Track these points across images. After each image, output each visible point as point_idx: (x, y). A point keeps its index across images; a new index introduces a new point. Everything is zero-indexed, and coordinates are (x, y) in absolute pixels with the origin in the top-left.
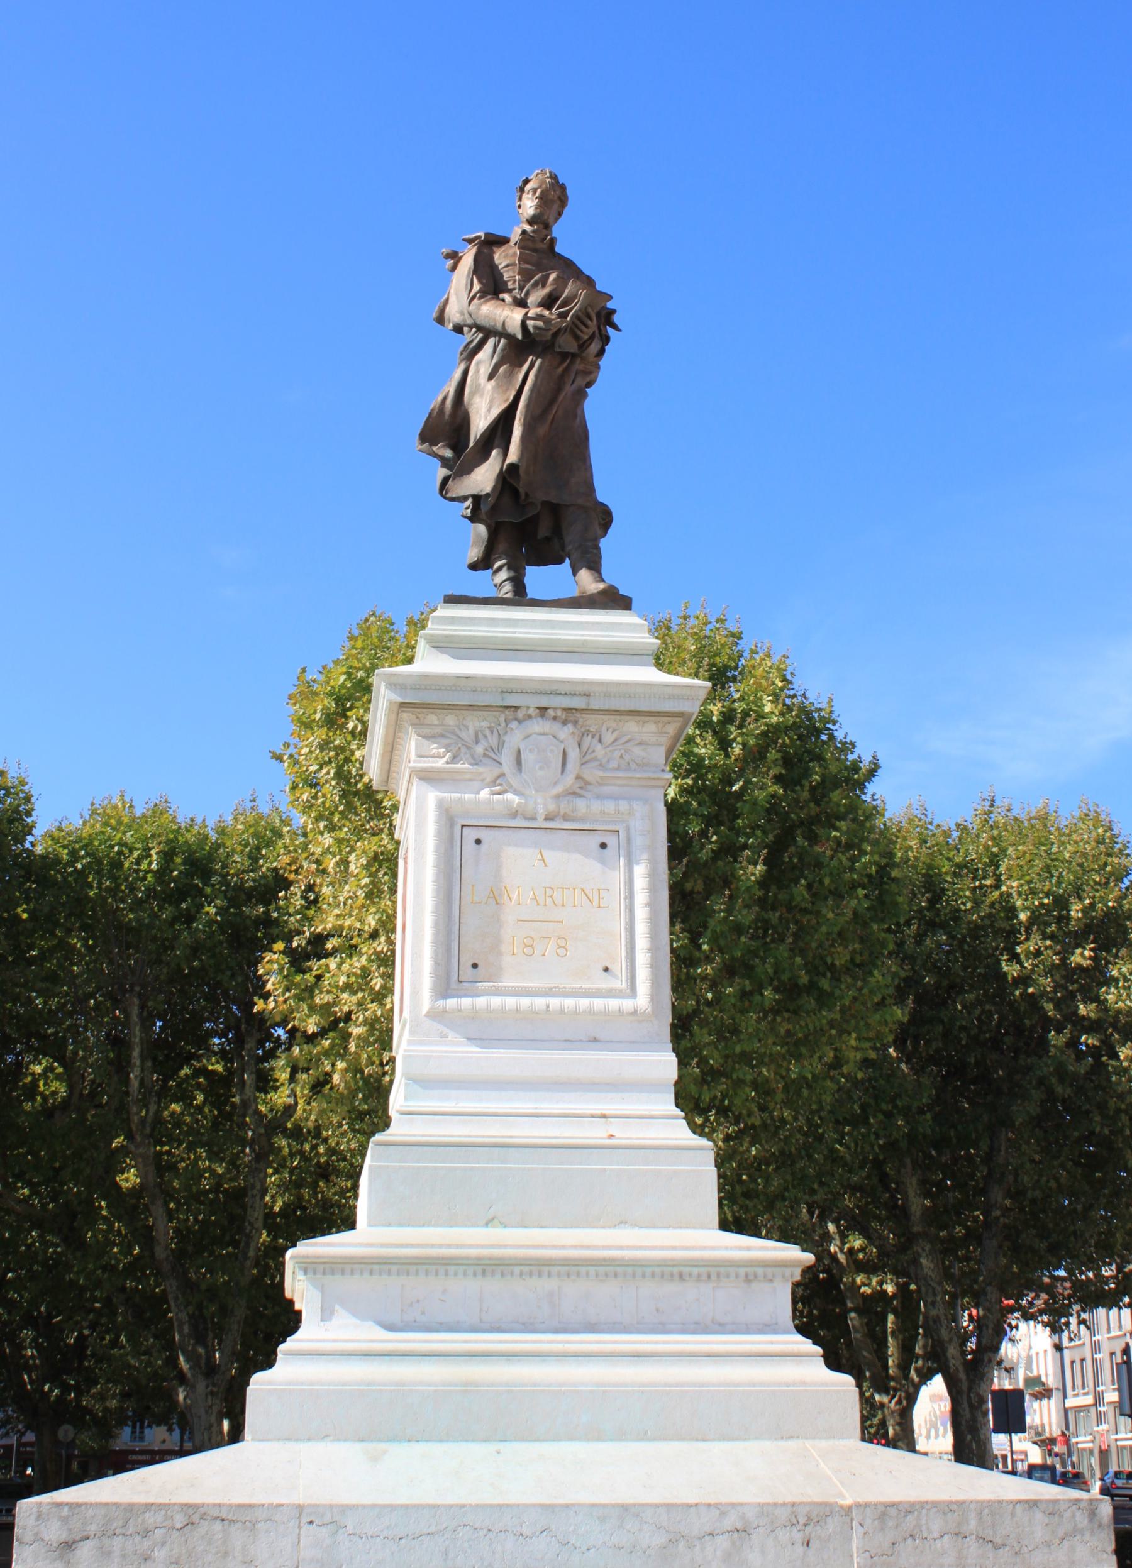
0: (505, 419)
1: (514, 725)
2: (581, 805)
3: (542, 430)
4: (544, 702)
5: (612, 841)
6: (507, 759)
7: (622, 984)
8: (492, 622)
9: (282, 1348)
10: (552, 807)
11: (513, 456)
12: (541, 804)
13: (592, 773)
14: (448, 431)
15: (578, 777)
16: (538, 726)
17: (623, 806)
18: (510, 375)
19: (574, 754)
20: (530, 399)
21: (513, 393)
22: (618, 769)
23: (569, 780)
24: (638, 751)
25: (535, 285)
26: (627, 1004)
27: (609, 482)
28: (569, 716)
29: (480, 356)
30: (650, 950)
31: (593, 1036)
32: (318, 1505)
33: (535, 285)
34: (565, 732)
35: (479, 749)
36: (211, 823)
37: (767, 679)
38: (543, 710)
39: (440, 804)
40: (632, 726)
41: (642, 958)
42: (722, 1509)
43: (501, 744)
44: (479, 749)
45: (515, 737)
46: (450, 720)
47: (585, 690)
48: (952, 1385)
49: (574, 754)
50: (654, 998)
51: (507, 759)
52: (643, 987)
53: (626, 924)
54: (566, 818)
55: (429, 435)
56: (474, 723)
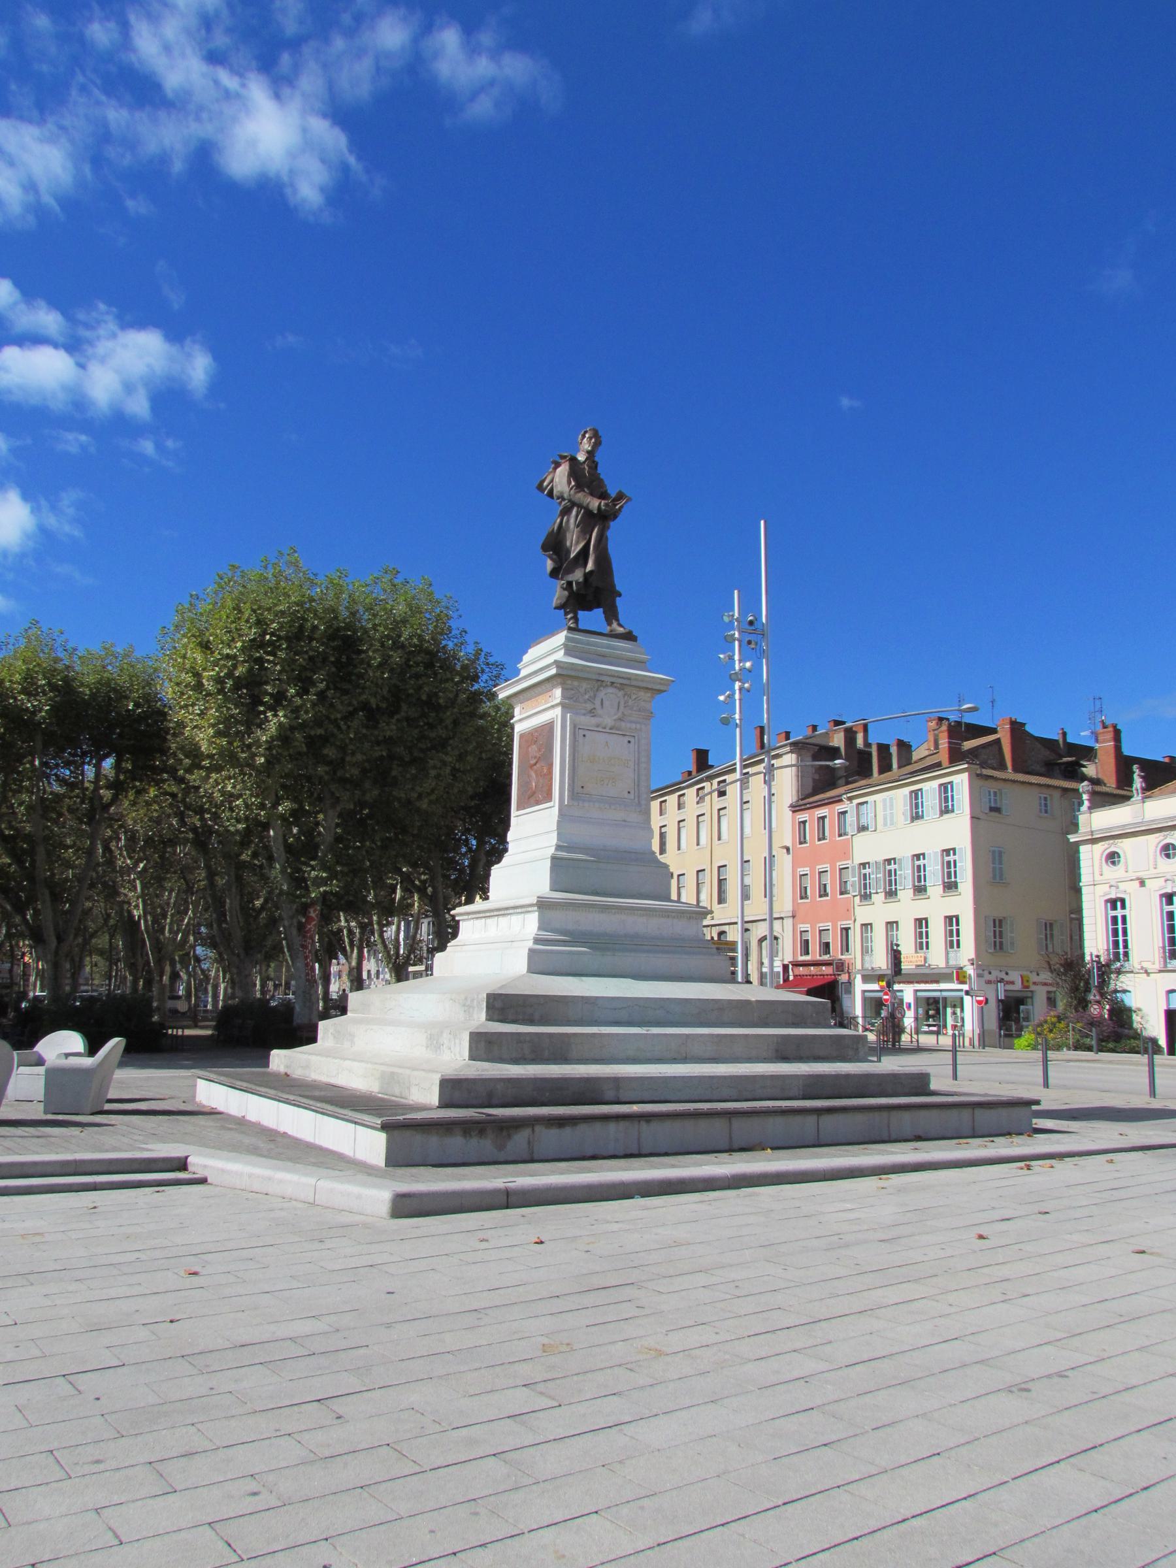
0: (586, 548)
2: (623, 724)
4: (613, 680)
5: (632, 740)
6: (598, 702)
12: (609, 721)
14: (555, 544)
16: (610, 690)
17: (638, 726)
23: (620, 714)
27: (620, 583)
28: (622, 687)
32: (314, 1164)
34: (621, 693)
37: (162, 909)
38: (613, 683)
39: (549, 727)
40: (642, 694)
43: (595, 696)
45: (602, 694)
46: (576, 683)
47: (629, 677)
51: (598, 702)
53: (82, 1162)
55: (545, 547)
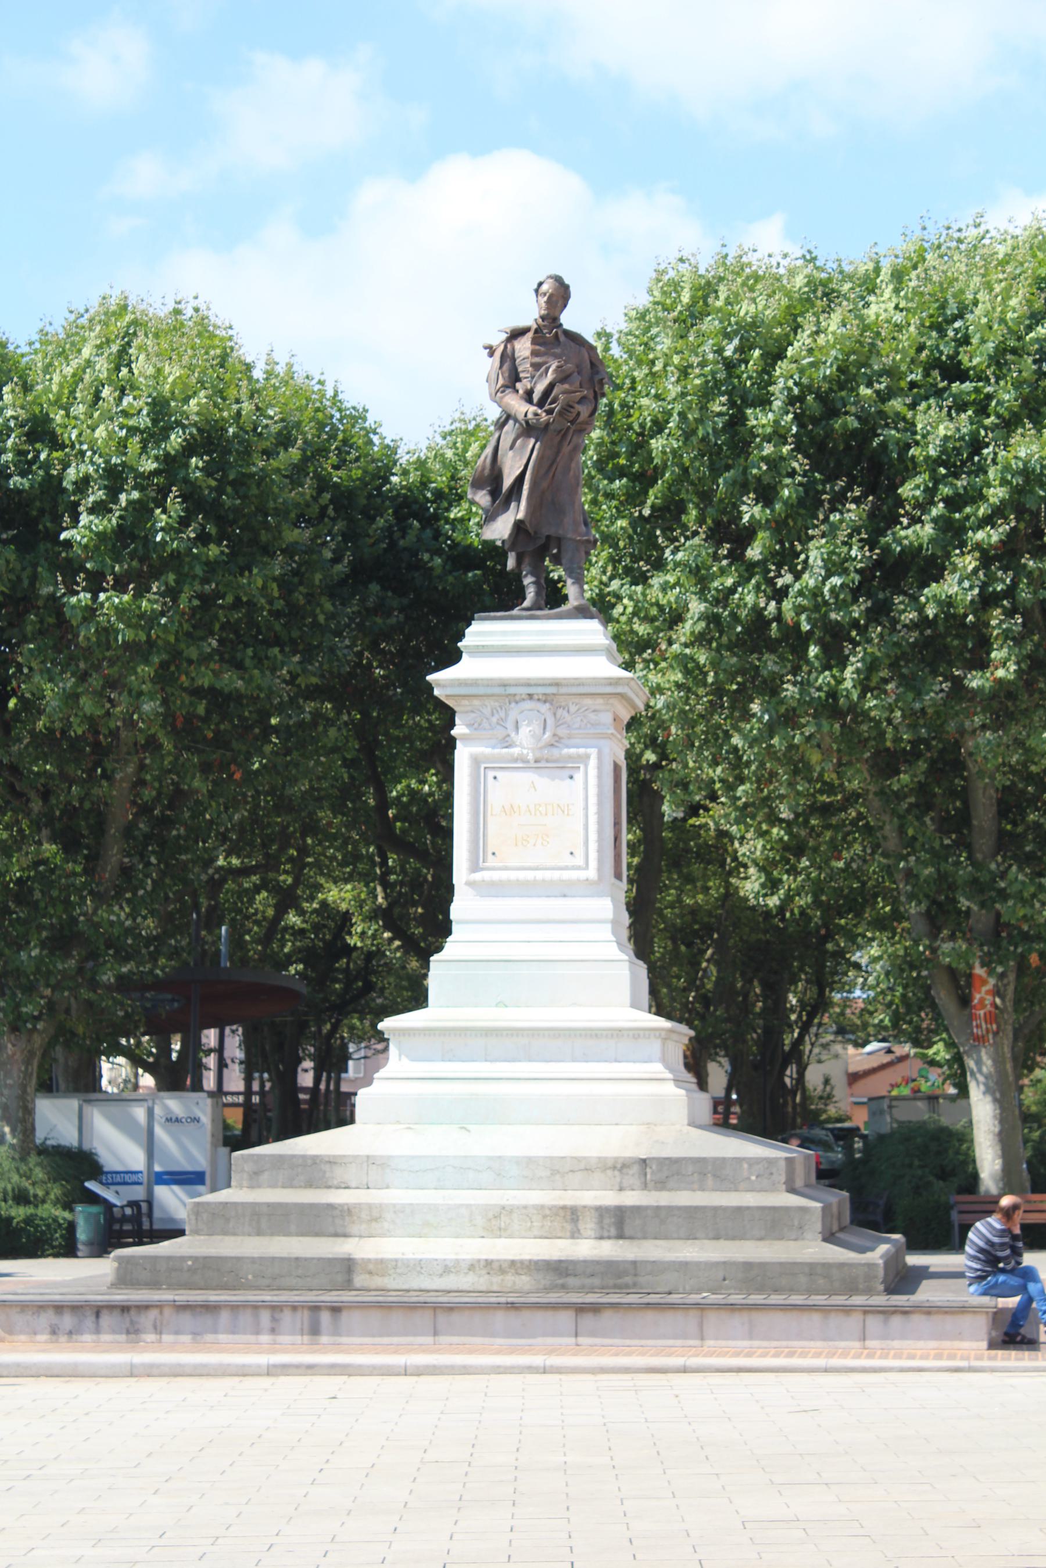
0: (520, 479)
1: (513, 705)
2: (555, 752)
3: (545, 484)
4: (531, 690)
6: (510, 725)
7: (579, 861)
8: (504, 633)
9: (376, 1076)
10: (538, 755)
11: (521, 516)
13: (562, 732)
15: (555, 735)
16: (528, 705)
18: (523, 446)
19: (550, 722)
20: (532, 474)
21: (524, 461)
22: (580, 728)
24: (592, 716)
25: (541, 375)
26: (582, 875)
28: (546, 699)
29: (506, 428)
30: (543, 880)
31: (564, 890)
33: (541, 375)
34: (545, 708)
35: (494, 720)
36: (423, 445)
38: (530, 696)
40: (588, 701)
41: (593, 846)
42: (578, 1159)
43: (507, 715)
44: (494, 720)
45: (514, 711)
48: (33, 1141)
49: (550, 722)
50: (600, 870)
51: (510, 725)
52: (593, 863)
54: (547, 761)
56: (491, 703)
